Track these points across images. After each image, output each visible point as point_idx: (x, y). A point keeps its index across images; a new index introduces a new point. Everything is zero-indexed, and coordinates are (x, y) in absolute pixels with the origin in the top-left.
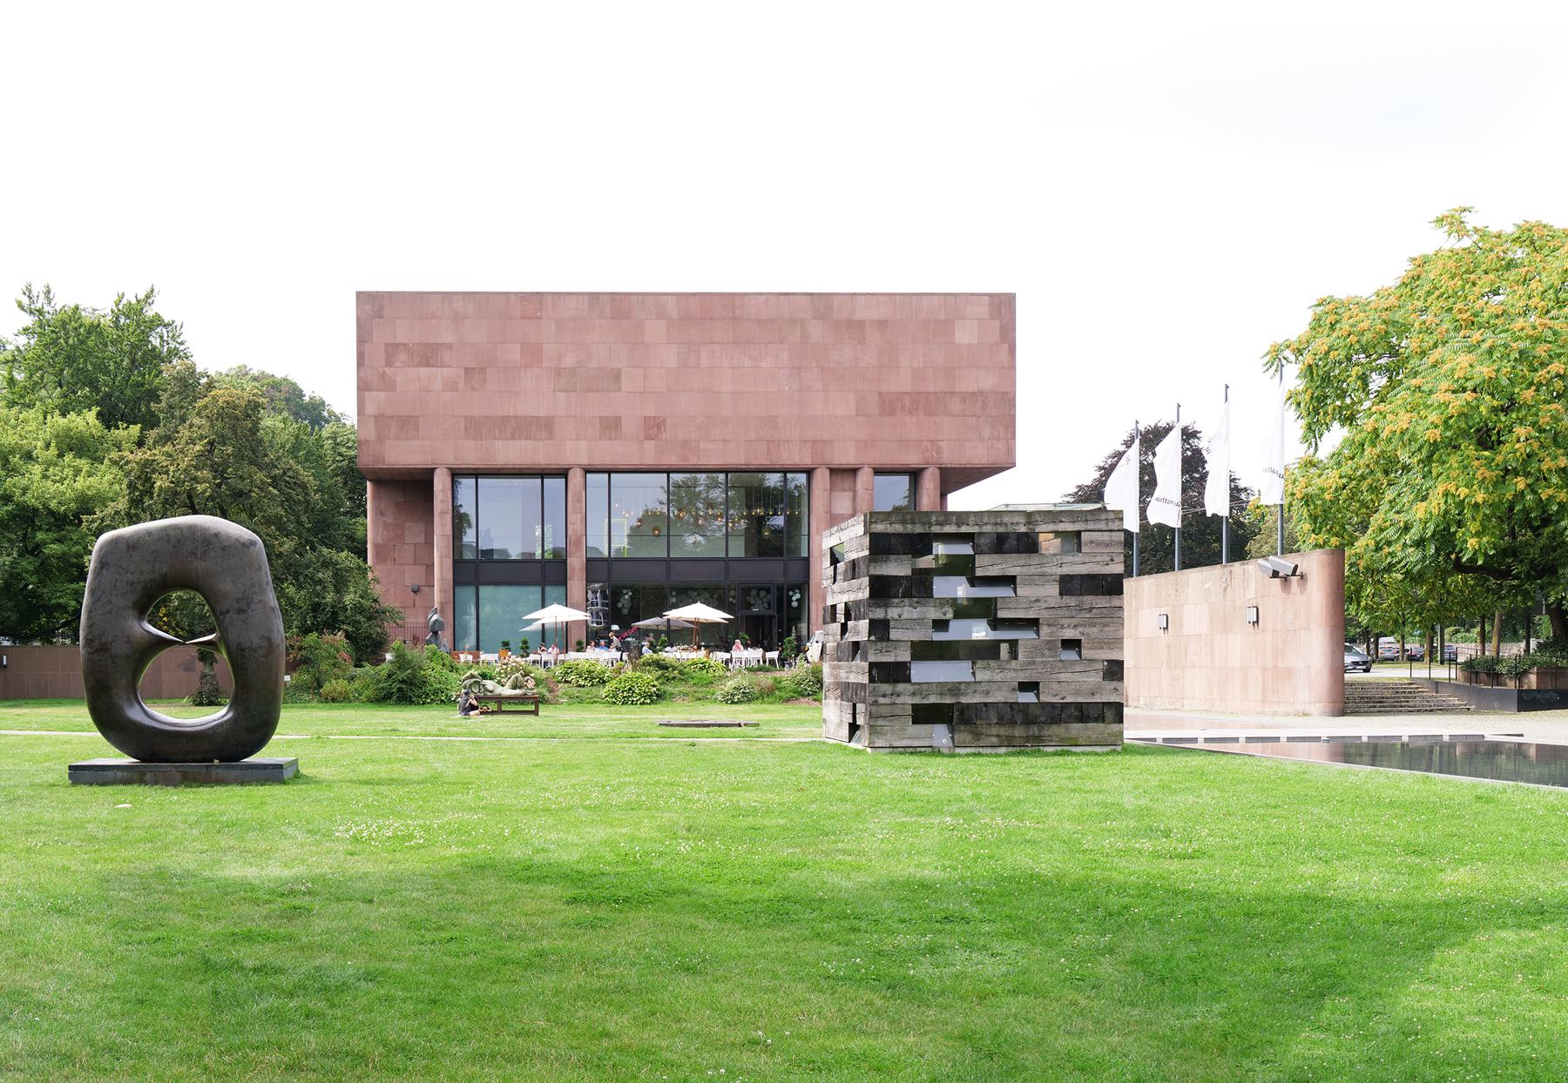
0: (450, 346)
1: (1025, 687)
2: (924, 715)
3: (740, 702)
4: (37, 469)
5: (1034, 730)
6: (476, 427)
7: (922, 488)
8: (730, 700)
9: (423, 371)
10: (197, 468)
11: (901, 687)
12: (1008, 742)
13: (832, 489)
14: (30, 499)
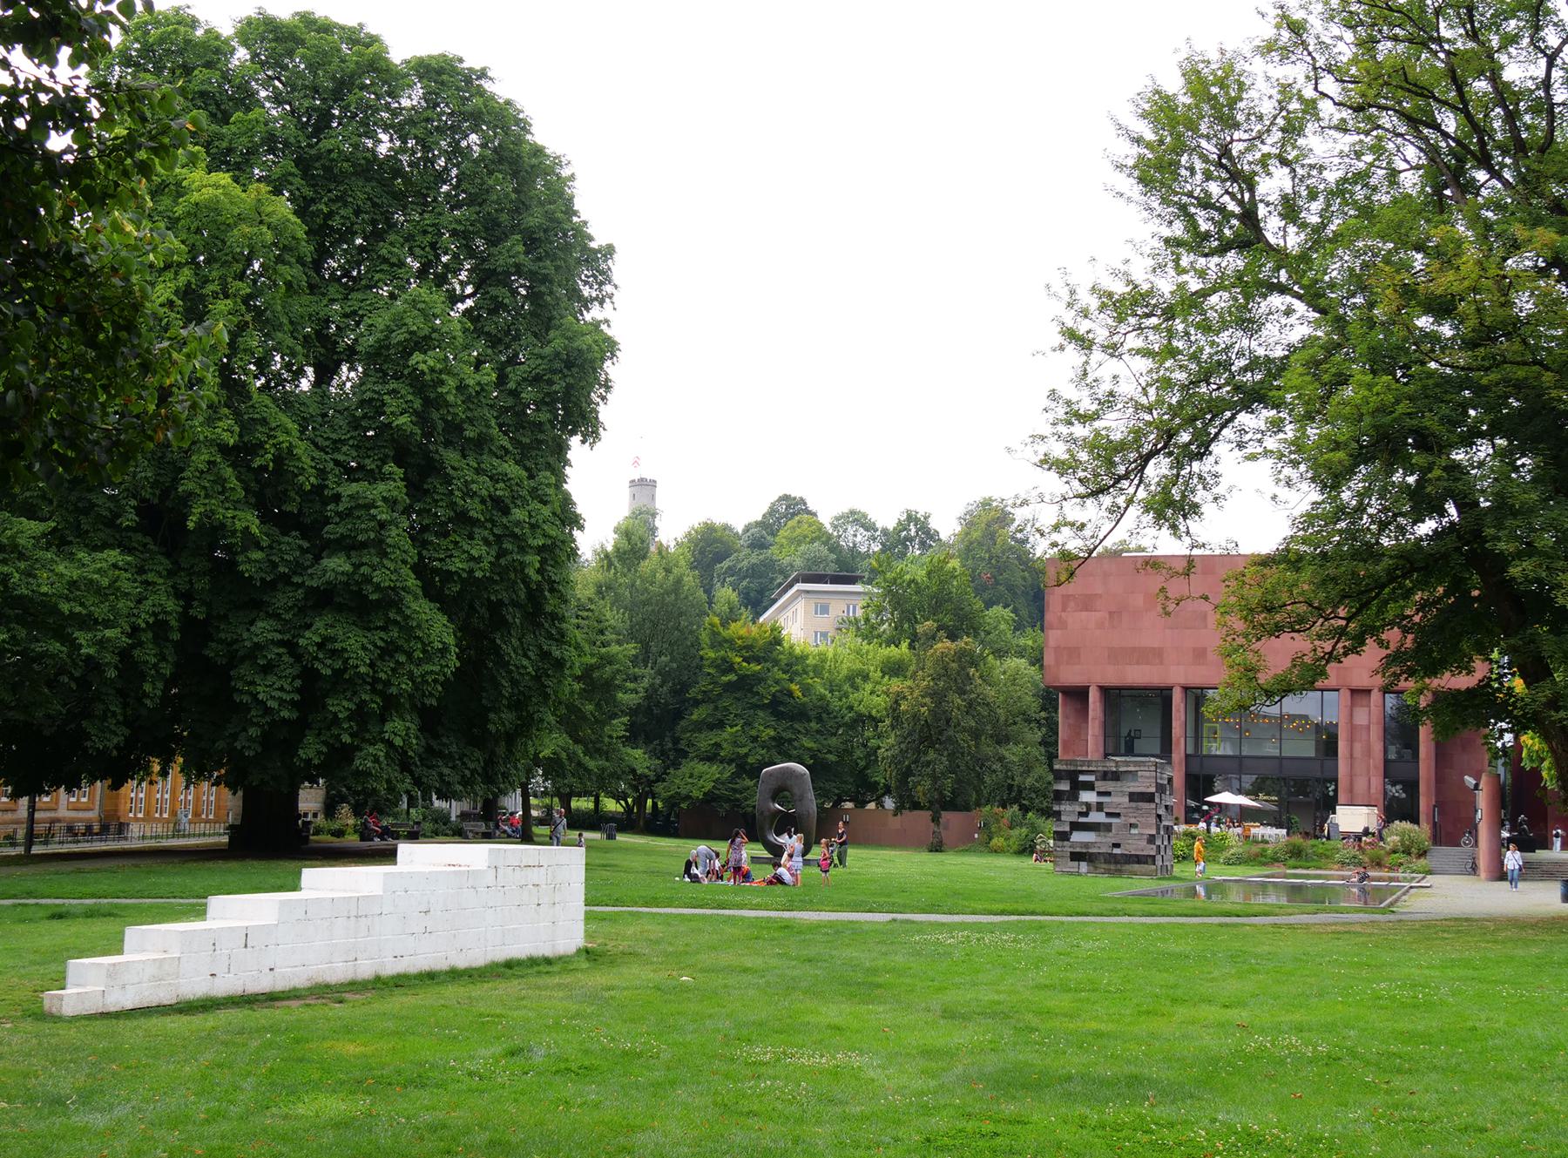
0: (1101, 596)
1: (1117, 845)
2: (1076, 857)
3: (1233, 864)
4: (869, 687)
5: (1119, 867)
6: (1117, 655)
7: (186, 861)
8: (1228, 863)
9: (1084, 614)
10: (923, 697)
11: (1066, 843)
12: (1108, 872)
13: (1353, 705)
14: (862, 709)
